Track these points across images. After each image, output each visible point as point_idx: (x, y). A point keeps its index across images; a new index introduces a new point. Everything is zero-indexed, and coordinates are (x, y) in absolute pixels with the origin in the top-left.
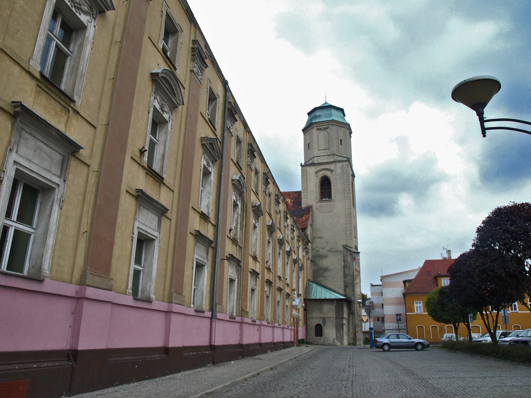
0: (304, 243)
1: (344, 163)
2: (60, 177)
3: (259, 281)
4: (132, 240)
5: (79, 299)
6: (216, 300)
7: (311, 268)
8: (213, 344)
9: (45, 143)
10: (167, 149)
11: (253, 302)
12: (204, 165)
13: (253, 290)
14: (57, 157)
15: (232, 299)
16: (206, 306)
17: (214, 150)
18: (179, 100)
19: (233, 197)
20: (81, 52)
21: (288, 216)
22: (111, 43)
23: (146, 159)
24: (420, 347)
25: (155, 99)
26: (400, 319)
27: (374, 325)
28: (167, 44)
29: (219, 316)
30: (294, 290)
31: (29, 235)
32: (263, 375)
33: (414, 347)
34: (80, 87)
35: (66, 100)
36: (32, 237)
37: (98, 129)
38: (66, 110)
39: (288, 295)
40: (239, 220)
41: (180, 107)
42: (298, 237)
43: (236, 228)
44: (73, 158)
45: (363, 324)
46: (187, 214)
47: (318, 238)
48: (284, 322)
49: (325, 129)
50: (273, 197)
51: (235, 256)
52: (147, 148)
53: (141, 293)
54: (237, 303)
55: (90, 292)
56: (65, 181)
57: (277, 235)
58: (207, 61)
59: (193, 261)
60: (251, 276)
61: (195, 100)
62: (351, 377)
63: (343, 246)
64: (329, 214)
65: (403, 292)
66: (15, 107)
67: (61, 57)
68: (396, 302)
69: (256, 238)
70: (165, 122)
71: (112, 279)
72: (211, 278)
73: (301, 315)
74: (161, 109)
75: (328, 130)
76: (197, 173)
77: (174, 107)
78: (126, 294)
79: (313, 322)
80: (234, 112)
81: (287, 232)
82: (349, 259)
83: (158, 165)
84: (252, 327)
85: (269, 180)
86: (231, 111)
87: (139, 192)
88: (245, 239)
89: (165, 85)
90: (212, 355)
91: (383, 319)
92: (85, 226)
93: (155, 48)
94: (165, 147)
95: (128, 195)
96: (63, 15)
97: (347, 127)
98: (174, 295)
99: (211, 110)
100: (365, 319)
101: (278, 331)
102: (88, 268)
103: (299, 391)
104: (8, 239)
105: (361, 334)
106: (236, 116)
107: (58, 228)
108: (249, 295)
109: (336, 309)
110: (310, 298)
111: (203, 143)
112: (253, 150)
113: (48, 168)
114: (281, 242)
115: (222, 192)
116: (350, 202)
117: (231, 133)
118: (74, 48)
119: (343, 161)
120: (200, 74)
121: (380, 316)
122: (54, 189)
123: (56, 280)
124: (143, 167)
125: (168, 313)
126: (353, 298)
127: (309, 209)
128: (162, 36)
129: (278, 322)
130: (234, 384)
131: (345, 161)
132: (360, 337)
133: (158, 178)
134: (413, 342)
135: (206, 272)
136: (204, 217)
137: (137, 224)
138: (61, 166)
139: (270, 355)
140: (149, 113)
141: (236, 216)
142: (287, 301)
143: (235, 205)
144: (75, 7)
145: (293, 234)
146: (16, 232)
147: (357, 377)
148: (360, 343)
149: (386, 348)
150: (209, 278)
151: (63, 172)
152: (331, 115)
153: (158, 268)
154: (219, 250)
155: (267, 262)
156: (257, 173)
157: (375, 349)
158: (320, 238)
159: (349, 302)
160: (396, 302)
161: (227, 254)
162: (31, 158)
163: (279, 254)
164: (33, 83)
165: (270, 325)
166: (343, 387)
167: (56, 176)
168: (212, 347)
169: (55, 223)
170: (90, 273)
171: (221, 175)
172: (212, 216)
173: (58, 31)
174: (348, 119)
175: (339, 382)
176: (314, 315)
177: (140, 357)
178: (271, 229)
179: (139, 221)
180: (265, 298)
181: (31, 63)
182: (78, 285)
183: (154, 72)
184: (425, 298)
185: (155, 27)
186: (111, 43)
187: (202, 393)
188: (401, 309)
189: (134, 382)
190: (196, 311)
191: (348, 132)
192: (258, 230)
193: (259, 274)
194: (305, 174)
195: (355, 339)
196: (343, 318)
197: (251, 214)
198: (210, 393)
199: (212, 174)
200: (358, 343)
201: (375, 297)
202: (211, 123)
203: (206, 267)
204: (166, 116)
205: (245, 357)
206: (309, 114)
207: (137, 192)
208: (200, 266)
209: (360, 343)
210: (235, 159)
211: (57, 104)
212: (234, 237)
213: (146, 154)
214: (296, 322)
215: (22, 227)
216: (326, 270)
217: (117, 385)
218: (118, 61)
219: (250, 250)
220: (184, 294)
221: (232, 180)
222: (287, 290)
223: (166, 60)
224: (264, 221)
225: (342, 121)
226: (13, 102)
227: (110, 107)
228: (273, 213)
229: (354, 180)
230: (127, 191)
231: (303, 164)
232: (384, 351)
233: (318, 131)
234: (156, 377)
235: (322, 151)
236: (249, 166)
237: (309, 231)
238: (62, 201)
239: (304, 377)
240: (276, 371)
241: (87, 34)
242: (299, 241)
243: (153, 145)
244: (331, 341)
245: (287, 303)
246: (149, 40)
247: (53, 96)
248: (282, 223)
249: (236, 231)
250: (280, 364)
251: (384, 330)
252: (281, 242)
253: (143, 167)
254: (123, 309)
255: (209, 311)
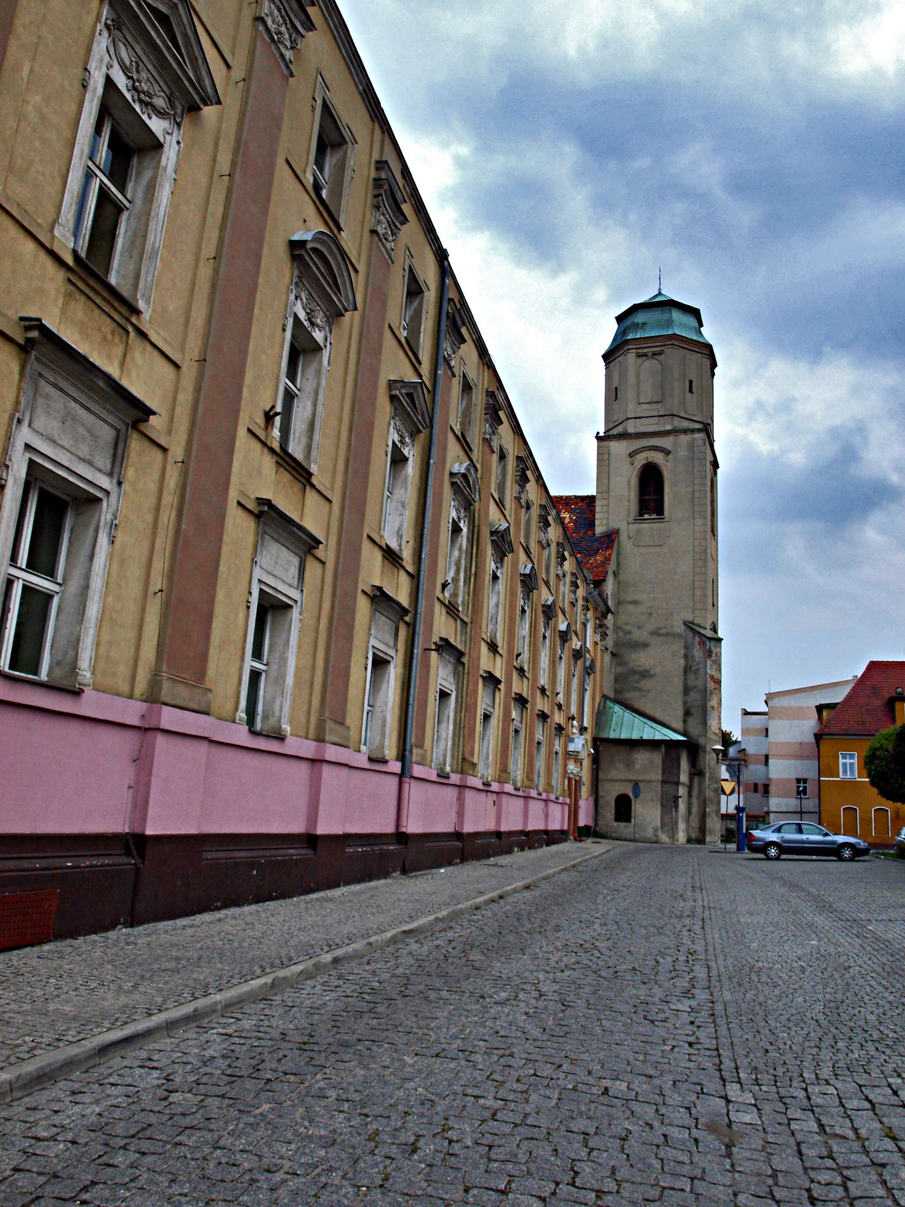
0: (599, 615)
1: (696, 435)
2: (110, 475)
3: (500, 697)
4: (248, 607)
5: (147, 730)
6: (412, 738)
7: (611, 670)
8: (404, 830)
9: (82, 405)
10: (320, 408)
11: (486, 743)
12: (394, 442)
13: (487, 717)
14: (107, 434)
15: (443, 735)
16: (390, 751)
17: (414, 408)
18: (347, 300)
19: (451, 512)
20: (151, 201)
21: (566, 554)
22: (212, 178)
23: (276, 433)
24: (847, 853)
25: (296, 299)
26: (804, 791)
27: (745, 800)
28: (321, 169)
29: (418, 771)
30: (573, 718)
31: (49, 597)
32: (511, 899)
33: (835, 852)
34: (149, 279)
35: (122, 308)
36: (56, 601)
37: (184, 369)
38: (122, 331)
39: (560, 729)
40: (463, 562)
41: (348, 314)
42: (586, 599)
43: (456, 580)
44: (135, 435)
45: (723, 798)
46: (358, 551)
47: (630, 603)
48: (549, 787)
49: (654, 354)
50: (535, 512)
51: (452, 641)
52: (279, 409)
53: (262, 721)
54: (453, 744)
55: (169, 718)
56: (120, 483)
57: (540, 595)
58: (407, 208)
59: (367, 653)
60: (484, 685)
61: (380, 296)
62: (699, 910)
63: (687, 624)
64: (657, 550)
65: (816, 731)
66: (27, 329)
67: (109, 210)
68: (798, 753)
69: (495, 600)
70: (318, 349)
71: (210, 690)
72: (403, 690)
73: (585, 774)
74: (309, 320)
75: (661, 358)
76: (381, 461)
77: (335, 315)
78: (234, 722)
79: (611, 792)
80: (459, 322)
81: (562, 589)
82: (698, 653)
83: (299, 443)
84: (482, 796)
85: (529, 473)
86: (454, 321)
87: (264, 504)
88: (473, 605)
89: (318, 267)
90: (400, 853)
91: (766, 787)
92: (157, 582)
93: (297, 182)
94: (315, 405)
95: (240, 512)
96: (113, 119)
97: (708, 349)
98: (329, 724)
99: (411, 318)
100: (728, 787)
101: (536, 807)
102: (164, 667)
103: (594, 934)
104: (11, 607)
105: (716, 819)
106: (464, 331)
107: (107, 583)
108: (479, 727)
109: (664, 762)
110: (605, 736)
111: (394, 392)
112: (498, 407)
113: (88, 457)
114: (549, 612)
115: (430, 501)
116: (705, 525)
117: (451, 368)
118: (135, 191)
119: (693, 431)
120: (391, 238)
121: (761, 782)
122: (99, 500)
123: (103, 692)
124: (272, 450)
125: (316, 762)
126: (701, 741)
127: (611, 537)
128: (312, 157)
129: (537, 786)
130: (455, 916)
131: (699, 430)
132: (715, 826)
133: (301, 474)
134: (834, 842)
135: (394, 673)
136: (391, 556)
137: (257, 574)
138: (111, 451)
139: (519, 857)
140: (284, 330)
141: (456, 553)
142: (557, 742)
143: (456, 530)
144: (141, 102)
145: (575, 592)
146: (27, 589)
147: (712, 911)
148: (714, 838)
149: (773, 852)
150: (398, 691)
151: (117, 464)
152: (669, 323)
153: (297, 668)
154: (420, 628)
155: (518, 655)
156: (502, 457)
157: (747, 854)
158: (635, 603)
159: (693, 749)
160: (798, 753)
161: (435, 639)
162: (56, 437)
163: (545, 637)
164: (60, 275)
165: (520, 793)
166: (684, 930)
167: (105, 473)
168: (401, 837)
169: (100, 573)
170: (169, 678)
171: (428, 464)
172: (407, 555)
173: (104, 156)
174: (708, 333)
175: (676, 921)
176: (614, 774)
177: (261, 853)
178: (529, 583)
179: (261, 567)
180: (512, 733)
181: (56, 233)
182: (145, 701)
183: (296, 237)
184: (866, 746)
185: (299, 136)
186: (212, 178)
187: (394, 931)
188: (808, 769)
189: (250, 904)
190: (371, 759)
191: (707, 363)
192: (501, 586)
193: (499, 682)
194: (606, 456)
195: (702, 829)
196: (678, 783)
197: (489, 550)
198: (410, 932)
199: (410, 463)
200: (708, 839)
201: (751, 738)
202: (410, 348)
203: (392, 665)
204: (318, 335)
205: (467, 860)
206: (620, 319)
207: (259, 504)
208: (380, 663)
209: (714, 838)
210: (457, 428)
211: (104, 317)
212: (452, 600)
213: (278, 419)
214: (574, 785)
215: (36, 580)
216: (645, 674)
217: (218, 909)
218: (225, 218)
219: (484, 629)
220: (348, 722)
221: (452, 474)
222: (559, 718)
223: (321, 208)
224: (515, 563)
225: (695, 338)
226: (22, 319)
227: (209, 322)
228: (534, 547)
229: (715, 473)
230: (239, 503)
231: (602, 434)
232: (769, 858)
233: (640, 360)
234: (290, 896)
235: (645, 406)
236: (487, 442)
237: (609, 587)
238: (114, 526)
239: (600, 907)
240: (537, 893)
241: (164, 161)
242: (588, 609)
243: (289, 397)
244: (649, 833)
245: (558, 746)
246: (286, 167)
247: (98, 301)
248: (552, 570)
249: (456, 588)
250: (544, 879)
251: (768, 813)
252: (549, 612)
253: (272, 450)
254: (230, 753)
255: (397, 760)
